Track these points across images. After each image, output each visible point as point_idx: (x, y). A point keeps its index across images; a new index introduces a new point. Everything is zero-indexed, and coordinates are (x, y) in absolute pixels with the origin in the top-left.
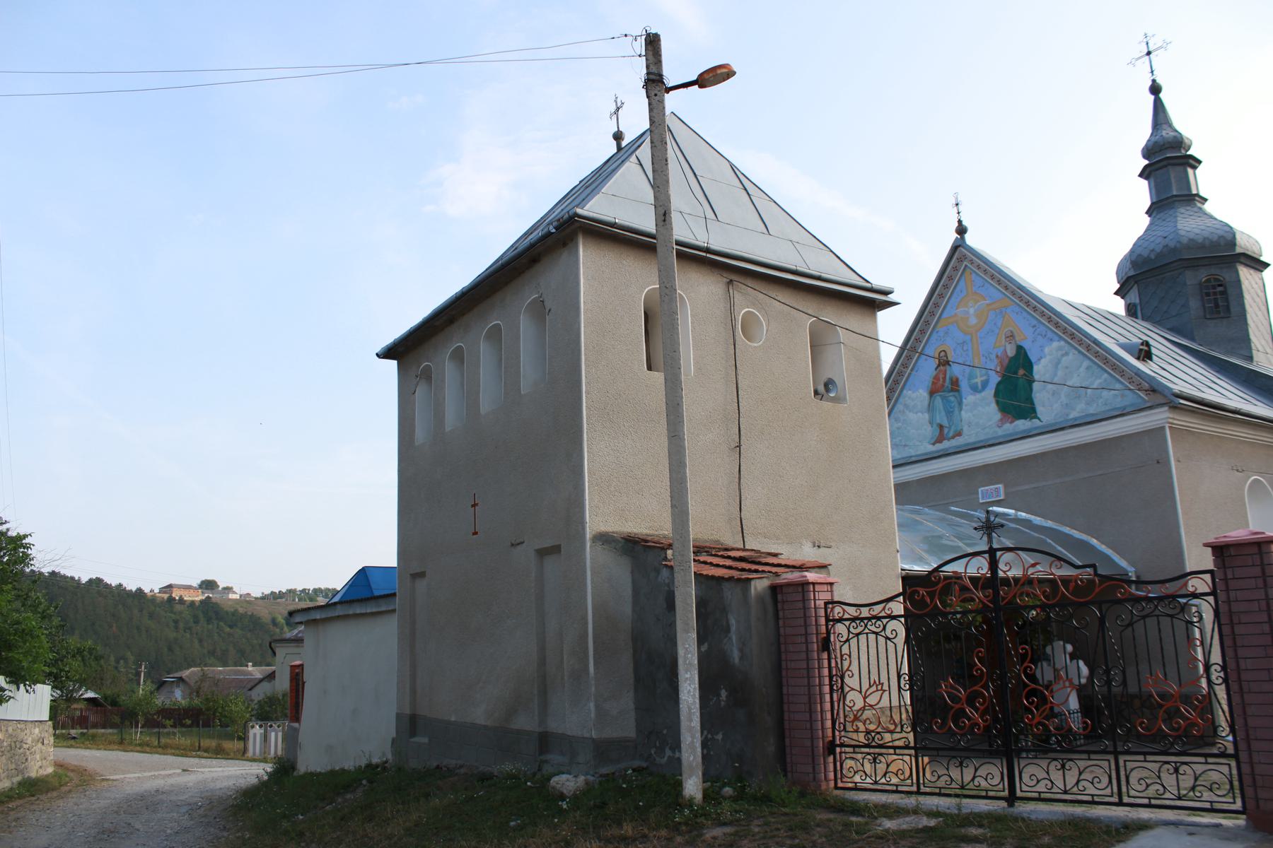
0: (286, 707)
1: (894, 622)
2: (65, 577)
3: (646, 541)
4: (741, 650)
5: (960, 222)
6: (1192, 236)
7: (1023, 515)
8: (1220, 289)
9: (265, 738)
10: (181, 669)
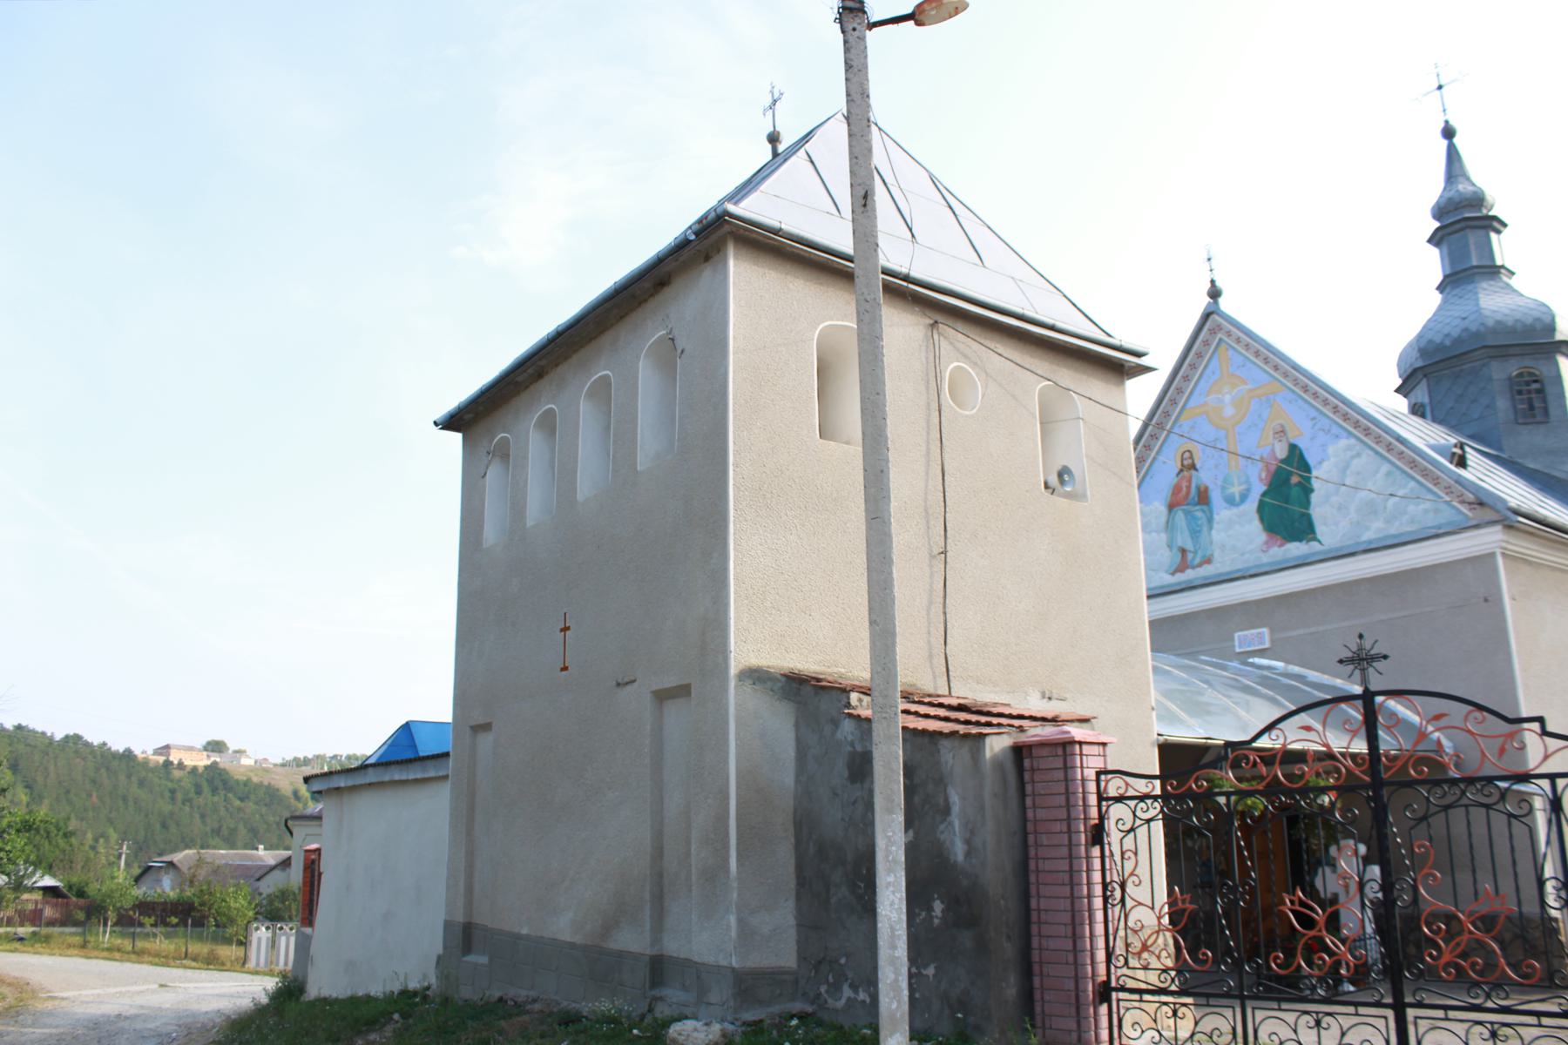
0: (299, 903)
1: (1119, 805)
2: (34, 732)
3: (818, 680)
4: (968, 842)
5: (1212, 282)
6: (1499, 317)
7: (1296, 669)
8: (1535, 386)
9: (273, 944)
10: (175, 850)
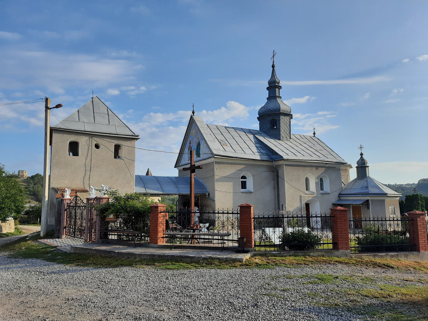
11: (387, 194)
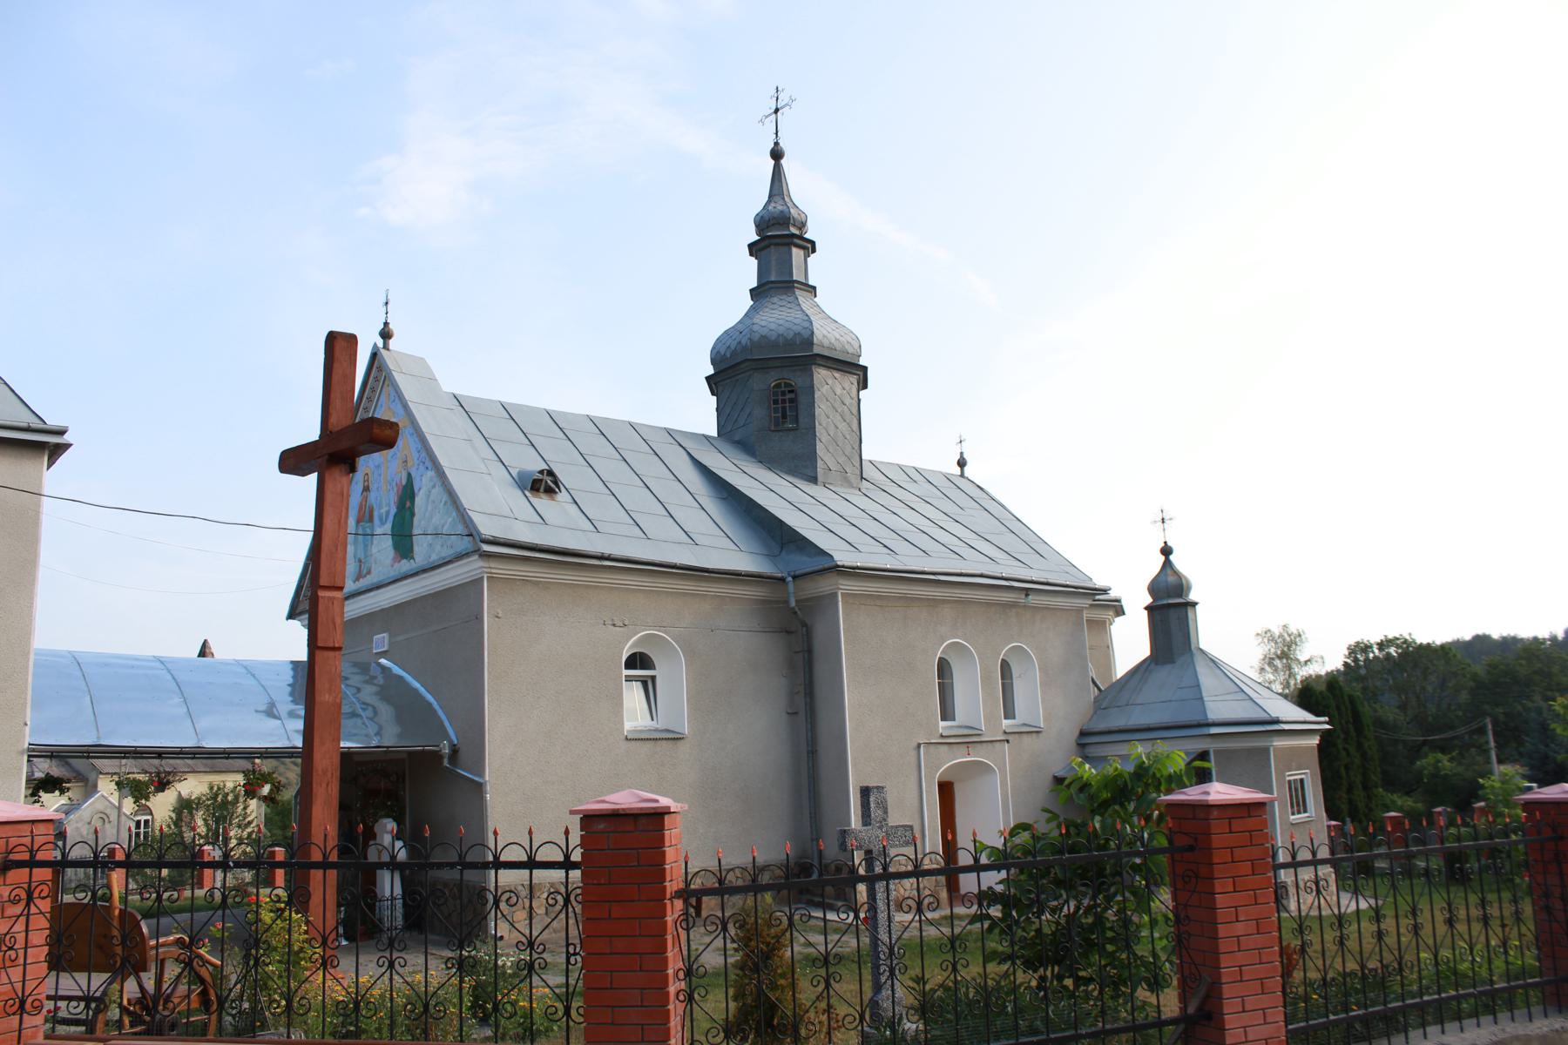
2: (1458, 645)
5: (386, 324)
8: (792, 396)
11: (1277, 721)
